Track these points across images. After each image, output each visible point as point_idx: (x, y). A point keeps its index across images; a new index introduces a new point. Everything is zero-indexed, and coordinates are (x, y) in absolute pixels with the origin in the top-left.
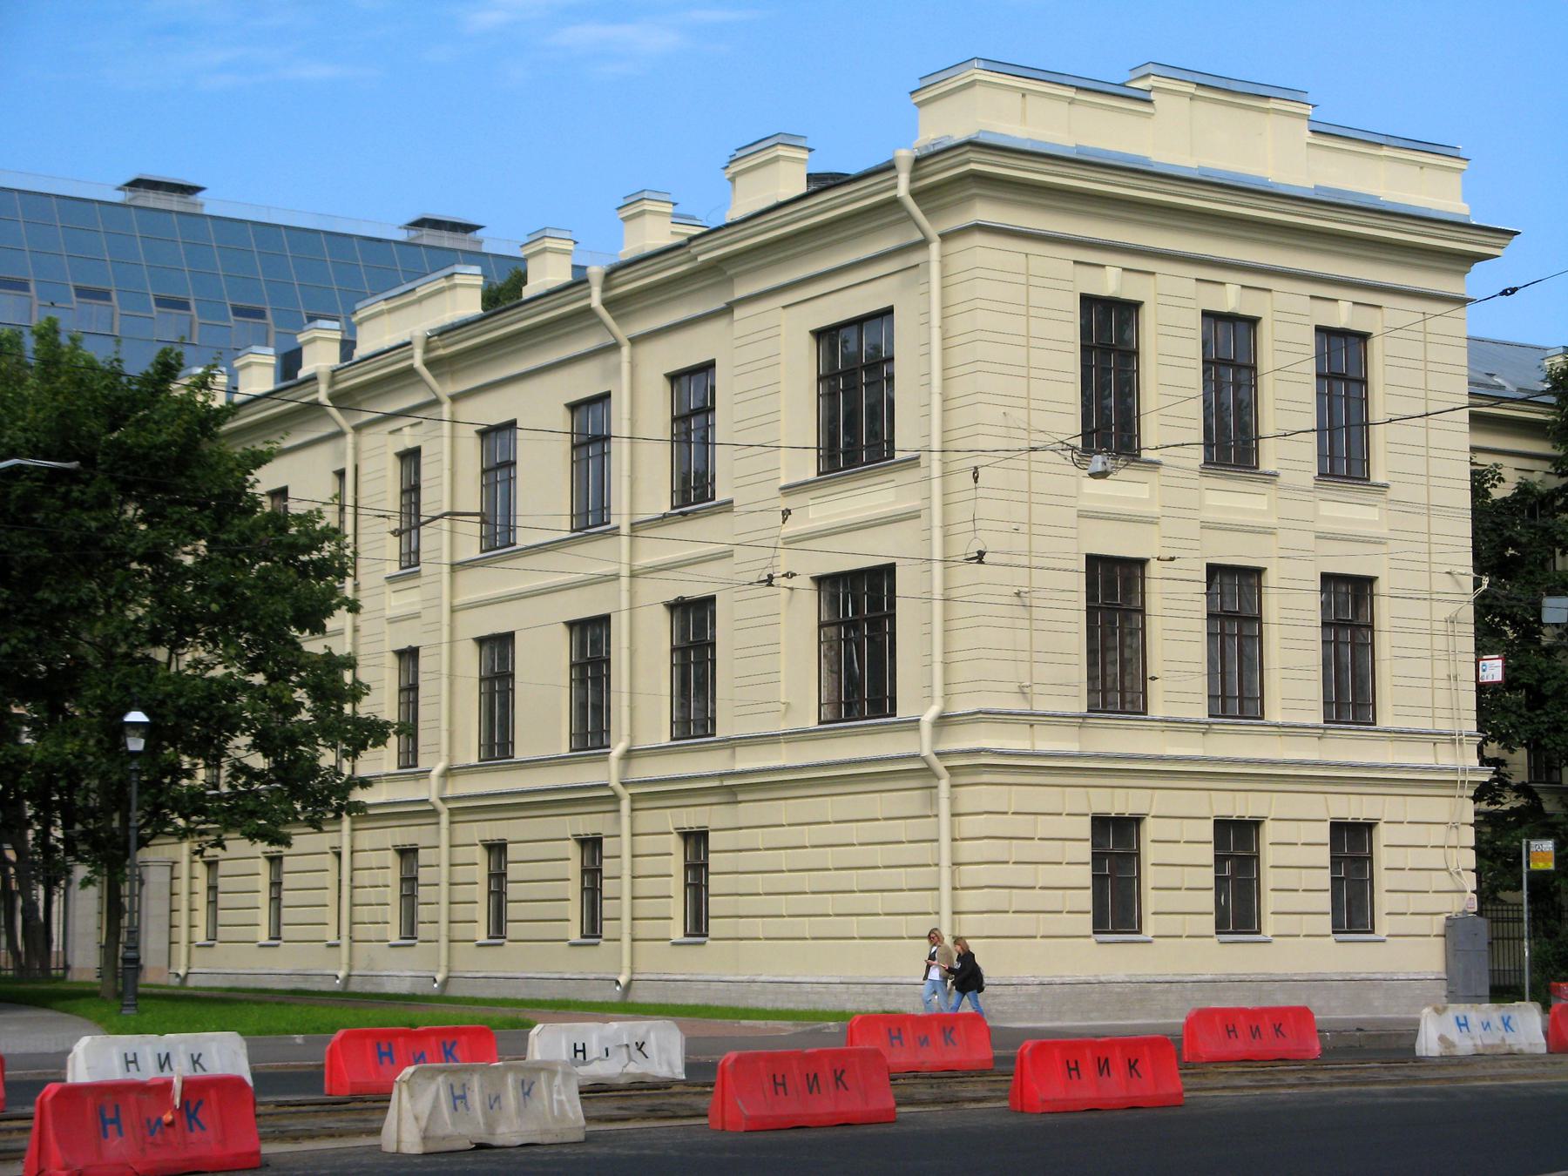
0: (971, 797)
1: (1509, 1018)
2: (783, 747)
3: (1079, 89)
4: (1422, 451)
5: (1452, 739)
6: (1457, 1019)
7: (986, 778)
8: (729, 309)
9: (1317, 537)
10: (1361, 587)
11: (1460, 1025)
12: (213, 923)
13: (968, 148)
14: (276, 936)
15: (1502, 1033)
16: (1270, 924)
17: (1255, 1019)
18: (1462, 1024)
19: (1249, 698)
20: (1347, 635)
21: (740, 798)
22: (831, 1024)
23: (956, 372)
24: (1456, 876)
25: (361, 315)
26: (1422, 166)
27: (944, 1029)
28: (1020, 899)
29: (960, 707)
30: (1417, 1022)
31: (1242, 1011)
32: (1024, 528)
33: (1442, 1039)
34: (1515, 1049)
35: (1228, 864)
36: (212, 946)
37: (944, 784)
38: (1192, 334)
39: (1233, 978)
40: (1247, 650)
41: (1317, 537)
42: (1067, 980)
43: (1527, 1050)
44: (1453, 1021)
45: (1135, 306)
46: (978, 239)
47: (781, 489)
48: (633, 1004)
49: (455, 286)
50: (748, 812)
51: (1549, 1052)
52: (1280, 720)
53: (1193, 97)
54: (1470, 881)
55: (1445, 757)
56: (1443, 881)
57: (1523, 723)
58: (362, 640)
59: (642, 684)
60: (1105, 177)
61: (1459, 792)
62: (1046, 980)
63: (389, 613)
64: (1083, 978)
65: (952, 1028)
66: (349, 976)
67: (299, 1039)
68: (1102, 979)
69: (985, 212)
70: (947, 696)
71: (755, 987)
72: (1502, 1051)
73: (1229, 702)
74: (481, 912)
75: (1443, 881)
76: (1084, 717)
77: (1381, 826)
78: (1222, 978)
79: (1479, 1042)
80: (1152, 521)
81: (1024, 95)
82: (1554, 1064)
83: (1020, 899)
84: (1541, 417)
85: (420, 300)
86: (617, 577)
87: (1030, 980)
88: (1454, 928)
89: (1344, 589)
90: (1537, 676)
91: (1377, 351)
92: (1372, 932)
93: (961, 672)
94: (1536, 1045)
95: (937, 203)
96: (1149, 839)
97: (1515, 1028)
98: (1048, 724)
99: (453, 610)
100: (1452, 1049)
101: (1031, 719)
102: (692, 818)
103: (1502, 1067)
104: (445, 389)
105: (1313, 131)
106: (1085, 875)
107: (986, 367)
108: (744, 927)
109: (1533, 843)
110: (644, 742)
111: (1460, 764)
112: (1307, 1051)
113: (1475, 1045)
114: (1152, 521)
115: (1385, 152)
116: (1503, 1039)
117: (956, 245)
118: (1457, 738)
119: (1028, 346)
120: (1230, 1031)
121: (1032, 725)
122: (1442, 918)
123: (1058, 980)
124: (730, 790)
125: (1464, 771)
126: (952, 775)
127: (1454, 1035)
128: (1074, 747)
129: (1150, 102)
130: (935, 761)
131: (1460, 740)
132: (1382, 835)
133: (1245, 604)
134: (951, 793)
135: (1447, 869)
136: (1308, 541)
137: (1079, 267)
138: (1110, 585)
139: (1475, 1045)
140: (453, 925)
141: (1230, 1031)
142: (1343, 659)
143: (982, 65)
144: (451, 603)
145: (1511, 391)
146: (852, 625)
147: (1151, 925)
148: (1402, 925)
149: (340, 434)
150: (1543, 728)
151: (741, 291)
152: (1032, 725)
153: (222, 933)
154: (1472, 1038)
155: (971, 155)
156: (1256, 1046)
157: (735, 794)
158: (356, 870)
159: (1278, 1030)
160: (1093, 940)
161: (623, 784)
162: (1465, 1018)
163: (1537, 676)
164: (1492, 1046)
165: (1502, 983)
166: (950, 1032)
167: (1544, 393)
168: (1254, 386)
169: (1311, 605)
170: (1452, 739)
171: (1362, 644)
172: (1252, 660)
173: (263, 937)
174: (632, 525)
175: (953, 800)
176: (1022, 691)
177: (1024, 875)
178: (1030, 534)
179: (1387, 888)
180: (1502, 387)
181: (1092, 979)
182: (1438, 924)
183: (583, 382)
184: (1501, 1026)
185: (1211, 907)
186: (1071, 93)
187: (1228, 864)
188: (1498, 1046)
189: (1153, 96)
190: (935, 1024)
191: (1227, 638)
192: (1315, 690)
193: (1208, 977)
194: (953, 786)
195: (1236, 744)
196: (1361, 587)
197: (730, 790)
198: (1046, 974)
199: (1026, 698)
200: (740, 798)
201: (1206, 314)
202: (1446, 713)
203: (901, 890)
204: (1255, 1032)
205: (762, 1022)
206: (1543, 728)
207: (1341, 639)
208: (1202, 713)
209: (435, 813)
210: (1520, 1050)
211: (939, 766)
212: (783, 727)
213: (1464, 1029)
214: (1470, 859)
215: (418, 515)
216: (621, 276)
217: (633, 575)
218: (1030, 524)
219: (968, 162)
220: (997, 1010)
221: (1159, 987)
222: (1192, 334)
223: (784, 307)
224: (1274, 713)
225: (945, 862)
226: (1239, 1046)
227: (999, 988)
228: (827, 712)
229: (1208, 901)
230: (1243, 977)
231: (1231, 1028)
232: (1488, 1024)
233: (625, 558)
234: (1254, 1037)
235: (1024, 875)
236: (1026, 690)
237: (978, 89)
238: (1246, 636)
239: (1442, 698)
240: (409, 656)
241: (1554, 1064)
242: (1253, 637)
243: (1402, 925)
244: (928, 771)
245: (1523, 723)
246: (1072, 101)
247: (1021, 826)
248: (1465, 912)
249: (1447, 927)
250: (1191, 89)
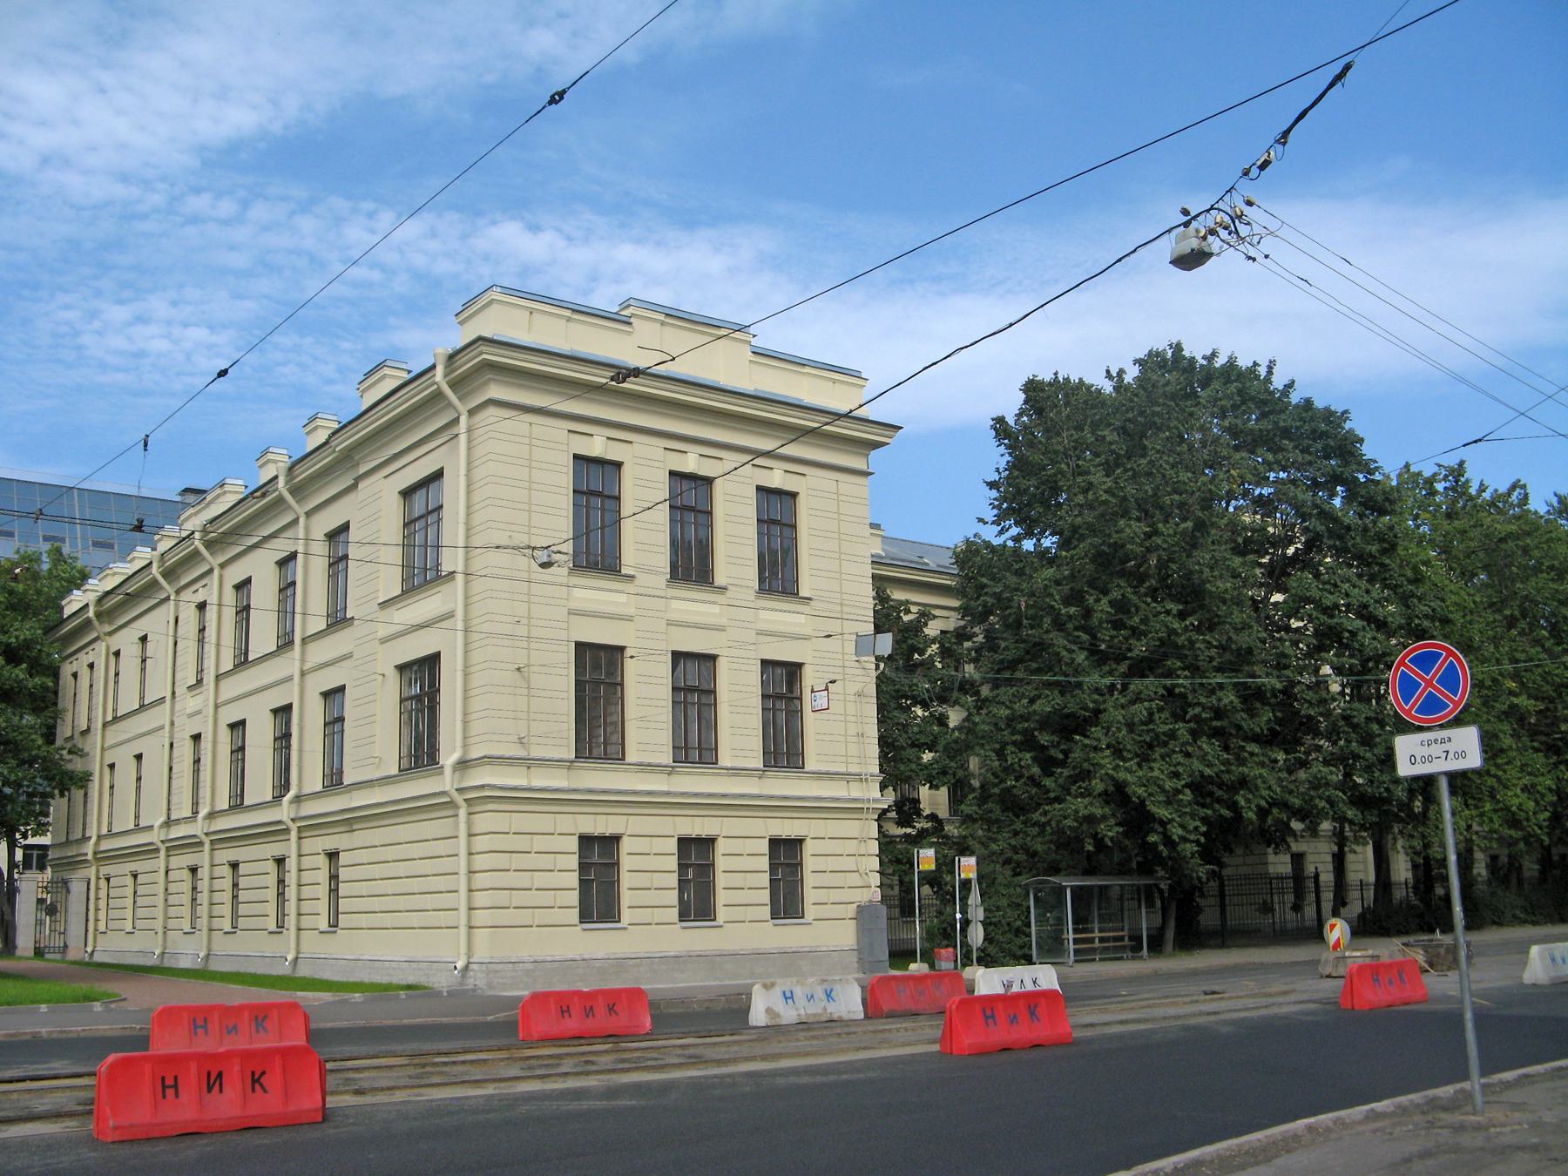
0: (484, 822)
1: (832, 990)
2: (377, 790)
3: (573, 310)
4: (837, 576)
5: (859, 778)
6: (784, 993)
7: (491, 807)
8: (354, 487)
9: (757, 634)
10: (793, 671)
11: (786, 998)
12: (235, 915)
13: (480, 342)
14: (334, 924)
15: (825, 1002)
16: (722, 914)
17: (587, 1001)
18: (788, 997)
19: (707, 749)
20: (782, 705)
21: (355, 827)
22: (357, 995)
23: (477, 507)
24: (864, 876)
25: (182, 518)
26: (835, 381)
27: (256, 1017)
28: (519, 898)
29: (475, 754)
30: (749, 996)
31: (579, 993)
32: (524, 621)
33: (769, 1011)
34: (835, 1016)
35: (691, 871)
36: (235, 932)
37: (462, 812)
38: (751, 542)
39: (691, 954)
40: (705, 714)
41: (757, 634)
42: (557, 958)
43: (846, 1016)
44: (780, 994)
45: (618, 465)
46: (492, 411)
47: (379, 604)
48: (303, 979)
49: (225, 493)
50: (362, 837)
51: (867, 1017)
52: (729, 765)
53: (663, 323)
54: (875, 879)
55: (856, 791)
56: (854, 879)
57: (921, 770)
58: (176, 730)
59: (307, 747)
60: (582, 368)
61: (864, 816)
62: (540, 959)
63: (189, 711)
64: (570, 956)
65: (265, 1017)
66: (163, 953)
67: (44, 1008)
68: (586, 957)
69: (496, 391)
70: (465, 746)
71: (360, 963)
72: (824, 1019)
73: (690, 752)
74: (323, 907)
75: (854, 879)
76: (571, 762)
77: (808, 839)
78: (683, 954)
79: (803, 1012)
80: (630, 619)
81: (531, 313)
82: (849, 1034)
83: (519, 898)
84: (949, 582)
85: (209, 504)
86: (290, 679)
87: (526, 959)
88: (863, 913)
89: (780, 671)
90: (931, 737)
91: (803, 506)
92: (803, 917)
93: (476, 728)
94: (854, 1012)
95: (465, 390)
96: (720, 853)
97: (836, 999)
98: (540, 766)
99: (217, 707)
100: (778, 1020)
101: (528, 762)
102: (330, 843)
103: (798, 1040)
104: (215, 561)
105: (753, 352)
106: (573, 879)
107: (497, 502)
108: (363, 920)
109: (921, 851)
110: (307, 790)
111: (866, 796)
112: (638, 1027)
113: (799, 1015)
114: (630, 619)
115: (807, 370)
116: (825, 1009)
117: (480, 417)
118: (864, 777)
119: (530, 489)
120: (564, 1011)
121: (529, 768)
122: (855, 905)
123: (549, 958)
124: (350, 821)
125: (869, 800)
126: (469, 806)
127: (780, 1006)
128: (563, 784)
129: (630, 324)
130: (455, 795)
131: (866, 779)
132: (809, 848)
133: (702, 681)
134: (468, 819)
135: (858, 871)
136: (752, 637)
137: (572, 435)
138: (596, 666)
139: (799, 1015)
140: (473, 911)
141: (564, 1011)
142: (778, 721)
143: (499, 289)
144: (216, 701)
145: (933, 566)
146: (418, 698)
147: (627, 916)
148: (738, 913)
149: (168, 599)
150: (934, 772)
151: (363, 469)
152: (529, 768)
153: (242, 923)
154: (797, 1009)
155: (483, 348)
156: (590, 1024)
157: (351, 825)
158: (472, 891)
159: (611, 1009)
160: (678, 926)
161: (292, 820)
162: (792, 992)
163: (931, 737)
164: (815, 1015)
165: (1332, 889)
166: (263, 1020)
167: (953, 564)
168: (710, 526)
169: (753, 678)
170: (859, 778)
171: (794, 711)
172: (708, 722)
173: (324, 926)
174: (303, 639)
175: (469, 824)
176: (521, 741)
177: (523, 880)
178: (529, 625)
179: (723, 886)
180: (927, 564)
181: (578, 957)
182: (851, 910)
183: (281, 547)
184: (824, 997)
185: (675, 901)
186: (568, 313)
187: (691, 871)
188: (820, 1015)
189: (632, 320)
190: (246, 1013)
191: (689, 706)
192: (756, 743)
193: (672, 954)
194: (470, 814)
195: (694, 782)
196: (793, 671)
197: (350, 821)
198: (540, 954)
199: (525, 749)
200: (355, 827)
201: (672, 474)
202: (856, 760)
203: (441, 892)
204: (589, 1011)
205: (311, 993)
206: (934, 772)
207: (778, 707)
208: (667, 758)
209: (201, 844)
210: (840, 1017)
211: (459, 799)
212: (377, 775)
213: (790, 1001)
214: (875, 863)
215: (246, 654)
216: (298, 469)
217: (303, 674)
218: (529, 618)
219: (482, 353)
220: (498, 983)
221: (631, 962)
222: (751, 542)
223: (385, 477)
224: (725, 759)
225: (463, 870)
226: (572, 1024)
227: (501, 966)
228: (405, 763)
229: (673, 897)
230: (700, 953)
231: (565, 1008)
232: (812, 996)
233: (297, 664)
234: (587, 1016)
235: (523, 880)
236: (524, 741)
237: (494, 306)
238: (704, 704)
239: (853, 750)
240: (197, 738)
241: (849, 1034)
242: (710, 705)
243: (738, 913)
244: (452, 804)
245: (921, 770)
246: (569, 320)
247: (521, 843)
248: (870, 901)
249: (858, 912)
250: (662, 317)
